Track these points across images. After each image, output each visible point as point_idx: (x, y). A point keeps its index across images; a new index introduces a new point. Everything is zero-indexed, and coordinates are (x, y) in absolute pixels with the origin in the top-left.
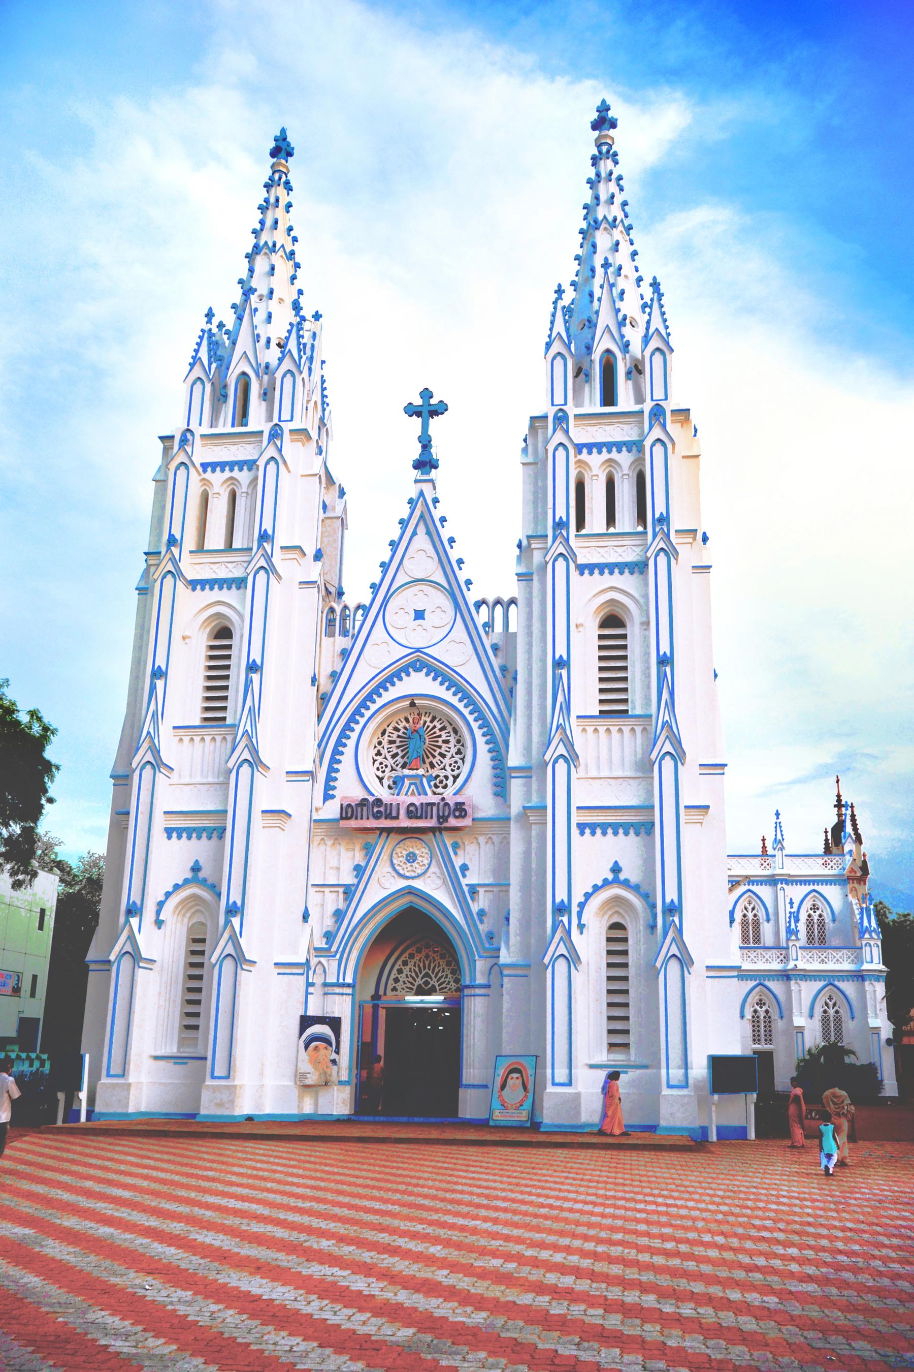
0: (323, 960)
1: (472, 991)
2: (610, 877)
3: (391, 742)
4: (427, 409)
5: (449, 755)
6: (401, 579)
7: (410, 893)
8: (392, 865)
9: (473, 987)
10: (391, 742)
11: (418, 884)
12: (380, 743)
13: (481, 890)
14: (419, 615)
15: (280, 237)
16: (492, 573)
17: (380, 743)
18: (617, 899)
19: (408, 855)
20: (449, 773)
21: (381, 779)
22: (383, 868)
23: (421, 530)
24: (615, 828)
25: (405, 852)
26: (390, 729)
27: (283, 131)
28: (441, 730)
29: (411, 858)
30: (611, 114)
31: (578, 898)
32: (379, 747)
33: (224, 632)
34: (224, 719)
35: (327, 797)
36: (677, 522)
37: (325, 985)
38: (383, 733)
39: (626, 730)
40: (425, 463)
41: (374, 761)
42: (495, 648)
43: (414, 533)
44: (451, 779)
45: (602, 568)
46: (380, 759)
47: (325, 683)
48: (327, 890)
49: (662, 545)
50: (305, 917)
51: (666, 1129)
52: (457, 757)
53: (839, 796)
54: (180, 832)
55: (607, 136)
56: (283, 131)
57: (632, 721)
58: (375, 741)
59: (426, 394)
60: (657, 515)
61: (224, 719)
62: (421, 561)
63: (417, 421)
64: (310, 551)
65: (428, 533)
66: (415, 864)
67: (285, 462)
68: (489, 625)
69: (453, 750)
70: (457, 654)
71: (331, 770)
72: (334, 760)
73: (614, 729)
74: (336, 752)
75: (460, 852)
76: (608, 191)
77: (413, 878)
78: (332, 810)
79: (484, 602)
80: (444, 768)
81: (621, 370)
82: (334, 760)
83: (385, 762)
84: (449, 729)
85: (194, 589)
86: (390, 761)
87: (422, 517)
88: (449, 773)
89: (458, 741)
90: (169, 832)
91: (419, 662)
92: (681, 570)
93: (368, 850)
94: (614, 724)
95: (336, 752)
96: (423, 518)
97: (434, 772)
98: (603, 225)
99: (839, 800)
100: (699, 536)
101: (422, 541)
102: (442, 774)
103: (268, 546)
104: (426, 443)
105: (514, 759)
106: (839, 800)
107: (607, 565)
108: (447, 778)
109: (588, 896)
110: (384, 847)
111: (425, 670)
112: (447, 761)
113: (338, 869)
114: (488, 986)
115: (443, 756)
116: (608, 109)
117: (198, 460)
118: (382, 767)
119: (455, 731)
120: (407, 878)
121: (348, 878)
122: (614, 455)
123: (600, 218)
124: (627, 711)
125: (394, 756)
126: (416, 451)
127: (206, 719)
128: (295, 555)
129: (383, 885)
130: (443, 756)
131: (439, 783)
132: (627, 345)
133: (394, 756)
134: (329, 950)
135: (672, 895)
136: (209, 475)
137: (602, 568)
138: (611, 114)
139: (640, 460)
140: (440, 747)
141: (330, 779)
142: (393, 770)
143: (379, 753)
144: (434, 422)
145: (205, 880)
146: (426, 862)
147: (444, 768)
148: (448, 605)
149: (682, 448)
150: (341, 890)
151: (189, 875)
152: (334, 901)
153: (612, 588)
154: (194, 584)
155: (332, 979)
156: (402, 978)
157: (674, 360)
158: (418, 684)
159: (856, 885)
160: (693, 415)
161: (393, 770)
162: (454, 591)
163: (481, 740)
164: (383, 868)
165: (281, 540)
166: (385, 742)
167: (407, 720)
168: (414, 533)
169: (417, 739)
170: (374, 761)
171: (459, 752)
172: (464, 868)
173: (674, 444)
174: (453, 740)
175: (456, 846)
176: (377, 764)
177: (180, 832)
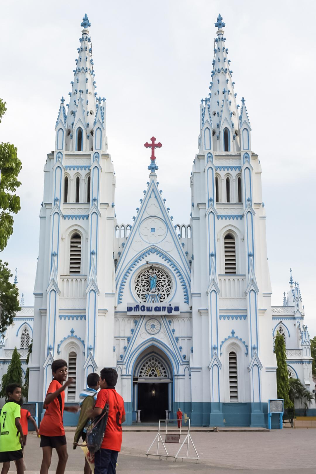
0: (120, 366)
1: (178, 377)
2: (231, 335)
3: (142, 280)
4: (153, 145)
5: (165, 286)
6: (146, 215)
7: (153, 340)
8: (146, 329)
9: (179, 376)
10: (142, 280)
11: (156, 337)
12: (138, 281)
13: (180, 339)
14: (153, 230)
15: (88, 65)
16: (181, 214)
17: (138, 281)
18: (233, 344)
19: (152, 325)
20: (165, 293)
21: (139, 295)
22: (142, 329)
23: (153, 196)
24: (233, 317)
25: (150, 325)
26: (142, 275)
27: (86, 15)
28: (162, 276)
29: (153, 326)
30: (223, 21)
31: (220, 343)
32: (138, 283)
33: (76, 236)
34: (79, 272)
35: (119, 303)
36: (255, 200)
37: (122, 375)
38: (139, 277)
39: (236, 280)
40: (153, 168)
41: (136, 288)
42: (183, 244)
43: (150, 197)
44: (166, 295)
45: (226, 217)
46: (138, 287)
47: (116, 257)
48: (120, 339)
49: (249, 210)
50: (114, 350)
51: (121, 359)
52: (168, 287)
53: (291, 278)
54: (65, 317)
55: (221, 31)
56: (86, 15)
57: (238, 277)
58: (136, 280)
59: (153, 139)
60: (247, 198)
61: (79, 272)
62: (153, 209)
63: (150, 150)
64: (110, 205)
65: (156, 197)
66: (154, 329)
67: (101, 169)
68: (180, 236)
69: (167, 284)
70: (168, 247)
71: (120, 292)
72: (121, 288)
73: (231, 280)
74: (122, 285)
75: (172, 324)
76: (223, 56)
77: (154, 334)
78: (123, 308)
79: (178, 226)
80: (163, 291)
81: (231, 135)
82: (121, 288)
83: (140, 288)
84: (165, 276)
85: (65, 219)
86: (142, 288)
87: (153, 190)
88: (165, 293)
89: (169, 281)
90: (60, 317)
91: (153, 250)
92: (256, 218)
93: (136, 322)
94: (231, 277)
95: (122, 285)
96: (153, 191)
97: (160, 292)
98: (221, 72)
99: (291, 280)
100: (262, 205)
101: (153, 200)
102: (163, 293)
103: (96, 203)
104: (153, 158)
105: (194, 289)
106: (291, 280)
107: (228, 216)
108: (164, 295)
109: (223, 342)
110: (142, 323)
111: (156, 253)
112: (164, 288)
113: (124, 330)
114: (184, 375)
115: (163, 286)
116: (222, 19)
117: (64, 165)
118: (139, 290)
119: (167, 277)
120: (152, 334)
121: (128, 334)
122: (230, 171)
123: (220, 68)
124: (235, 272)
125: (144, 286)
126: (149, 162)
127: (71, 272)
128: (105, 206)
129: (142, 338)
130: (163, 286)
131: (162, 298)
132: (233, 125)
133: (144, 286)
134: (122, 362)
135: (254, 343)
136: (68, 171)
137: (226, 217)
138: (223, 21)
139: (240, 174)
140: (162, 283)
141: (120, 295)
142: (143, 291)
143: (137, 285)
144: (157, 150)
145: (76, 336)
146: (159, 328)
147: (163, 291)
148: (163, 226)
149: (255, 171)
150: (126, 339)
151: (70, 334)
152: (123, 343)
153: (230, 225)
154: (64, 217)
155: (124, 373)
156: (145, 368)
157: (252, 133)
158: (154, 259)
159: (299, 320)
160: (259, 157)
161: (143, 291)
162: (166, 221)
163: (179, 281)
164: (142, 329)
165: (101, 201)
166: (140, 279)
167: (148, 272)
168: (150, 197)
169: (153, 278)
170: (136, 288)
171: (169, 285)
172: (174, 331)
173: (253, 169)
174: (166, 280)
175: (170, 322)
176: (137, 289)
177: (65, 317)
